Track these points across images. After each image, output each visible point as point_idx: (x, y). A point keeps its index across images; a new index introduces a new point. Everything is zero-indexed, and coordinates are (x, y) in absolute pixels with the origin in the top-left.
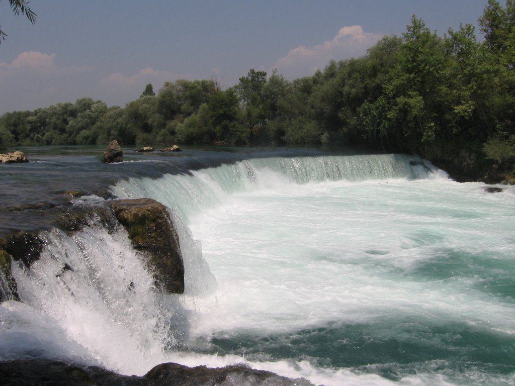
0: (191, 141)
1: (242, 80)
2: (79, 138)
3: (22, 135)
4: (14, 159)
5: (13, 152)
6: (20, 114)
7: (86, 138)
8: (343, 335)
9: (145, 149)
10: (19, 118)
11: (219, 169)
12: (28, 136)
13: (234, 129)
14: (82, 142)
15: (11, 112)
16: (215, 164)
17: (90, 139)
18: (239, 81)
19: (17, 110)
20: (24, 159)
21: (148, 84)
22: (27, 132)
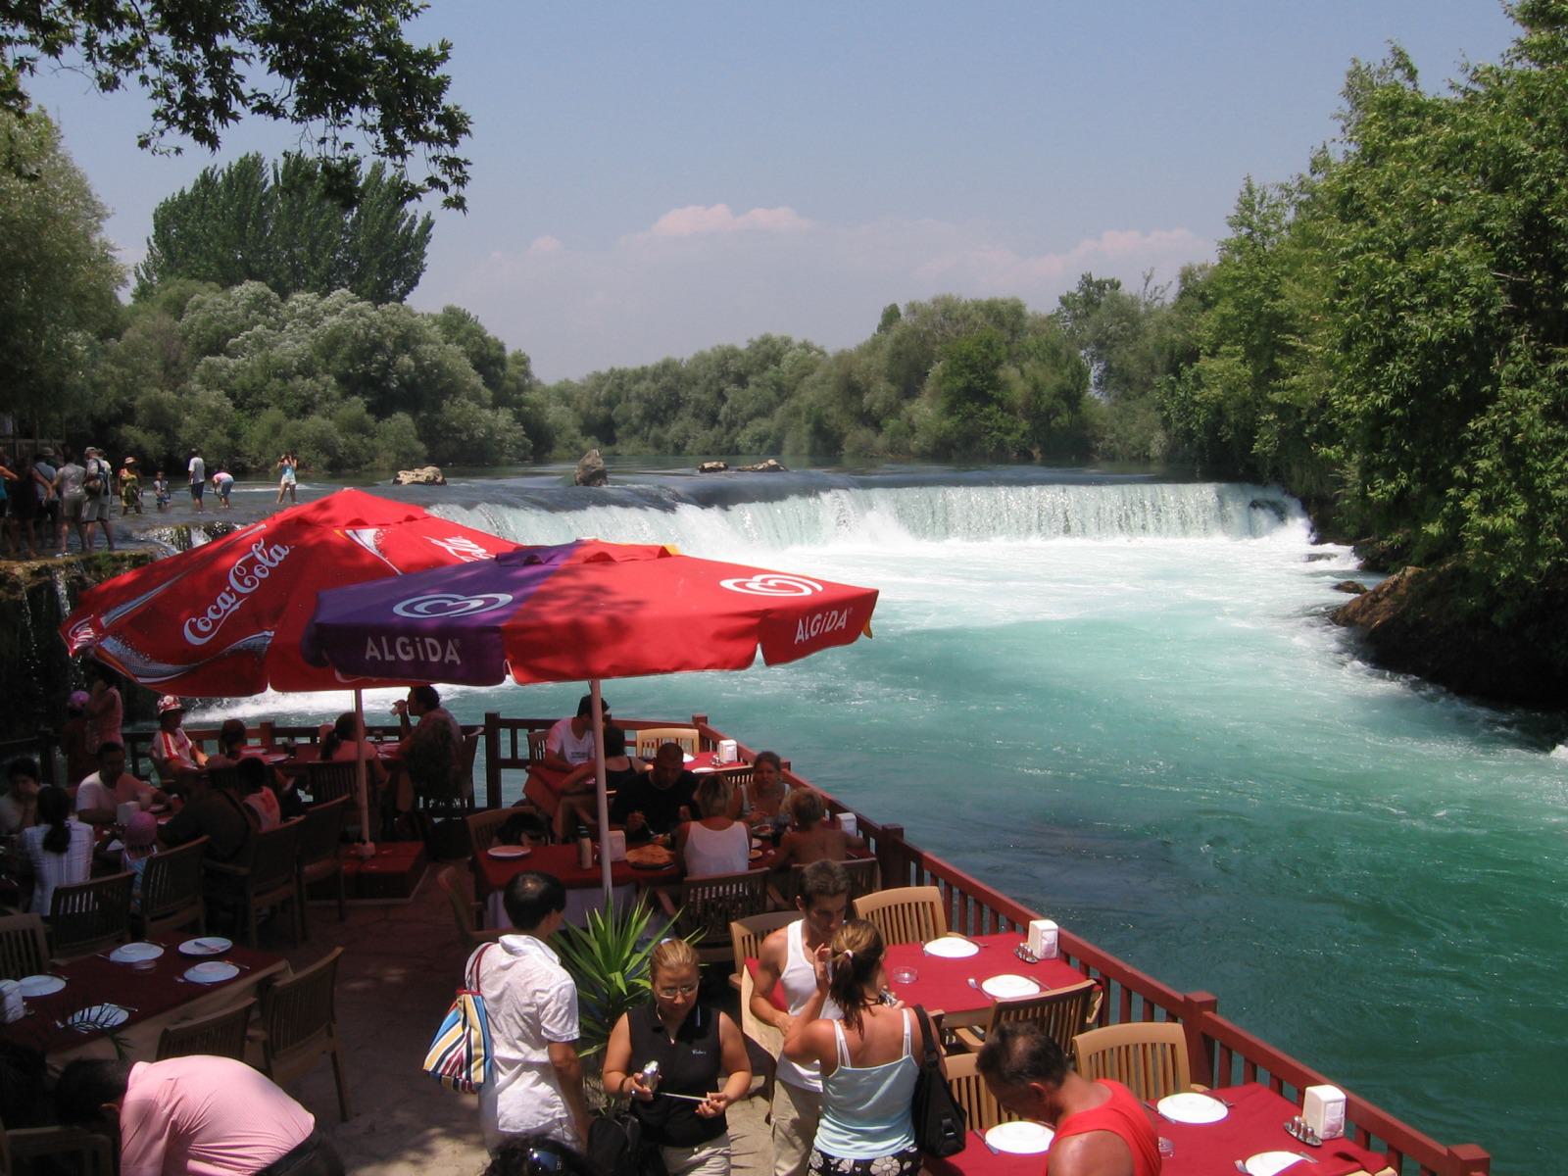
0: (925, 456)
1: (1064, 301)
2: (744, 439)
3: (624, 428)
4: (422, 479)
5: (422, 468)
6: (622, 375)
7: (761, 439)
8: (1300, 790)
9: (707, 465)
10: (620, 387)
11: (778, 508)
12: (635, 431)
13: (988, 423)
14: (750, 448)
15: (604, 370)
16: (771, 495)
17: (769, 442)
18: (1058, 304)
19: (619, 366)
20: (439, 479)
21: (888, 304)
22: (636, 421)
